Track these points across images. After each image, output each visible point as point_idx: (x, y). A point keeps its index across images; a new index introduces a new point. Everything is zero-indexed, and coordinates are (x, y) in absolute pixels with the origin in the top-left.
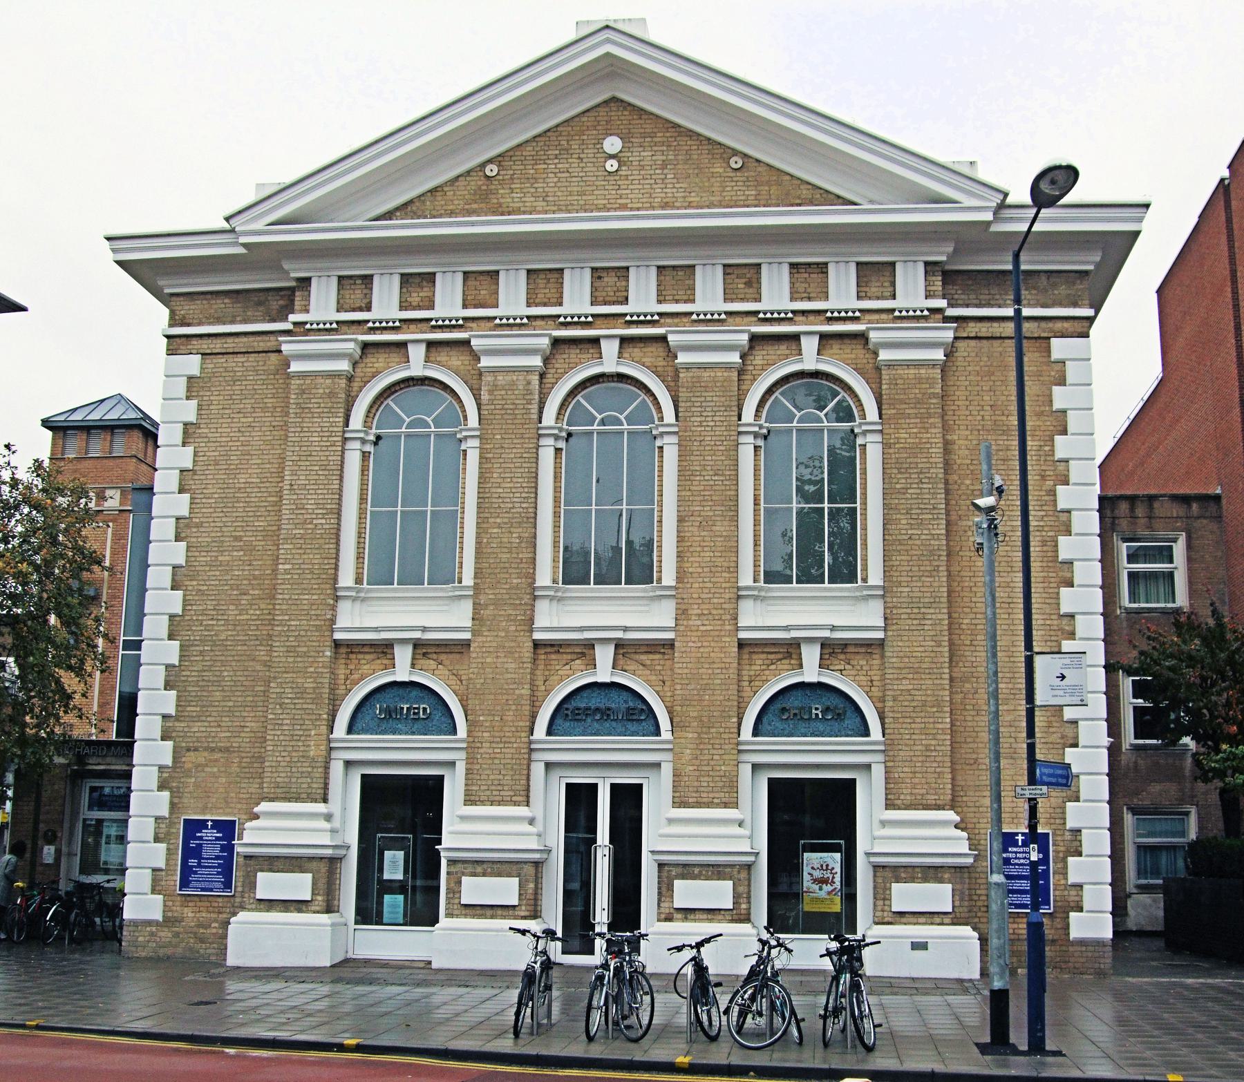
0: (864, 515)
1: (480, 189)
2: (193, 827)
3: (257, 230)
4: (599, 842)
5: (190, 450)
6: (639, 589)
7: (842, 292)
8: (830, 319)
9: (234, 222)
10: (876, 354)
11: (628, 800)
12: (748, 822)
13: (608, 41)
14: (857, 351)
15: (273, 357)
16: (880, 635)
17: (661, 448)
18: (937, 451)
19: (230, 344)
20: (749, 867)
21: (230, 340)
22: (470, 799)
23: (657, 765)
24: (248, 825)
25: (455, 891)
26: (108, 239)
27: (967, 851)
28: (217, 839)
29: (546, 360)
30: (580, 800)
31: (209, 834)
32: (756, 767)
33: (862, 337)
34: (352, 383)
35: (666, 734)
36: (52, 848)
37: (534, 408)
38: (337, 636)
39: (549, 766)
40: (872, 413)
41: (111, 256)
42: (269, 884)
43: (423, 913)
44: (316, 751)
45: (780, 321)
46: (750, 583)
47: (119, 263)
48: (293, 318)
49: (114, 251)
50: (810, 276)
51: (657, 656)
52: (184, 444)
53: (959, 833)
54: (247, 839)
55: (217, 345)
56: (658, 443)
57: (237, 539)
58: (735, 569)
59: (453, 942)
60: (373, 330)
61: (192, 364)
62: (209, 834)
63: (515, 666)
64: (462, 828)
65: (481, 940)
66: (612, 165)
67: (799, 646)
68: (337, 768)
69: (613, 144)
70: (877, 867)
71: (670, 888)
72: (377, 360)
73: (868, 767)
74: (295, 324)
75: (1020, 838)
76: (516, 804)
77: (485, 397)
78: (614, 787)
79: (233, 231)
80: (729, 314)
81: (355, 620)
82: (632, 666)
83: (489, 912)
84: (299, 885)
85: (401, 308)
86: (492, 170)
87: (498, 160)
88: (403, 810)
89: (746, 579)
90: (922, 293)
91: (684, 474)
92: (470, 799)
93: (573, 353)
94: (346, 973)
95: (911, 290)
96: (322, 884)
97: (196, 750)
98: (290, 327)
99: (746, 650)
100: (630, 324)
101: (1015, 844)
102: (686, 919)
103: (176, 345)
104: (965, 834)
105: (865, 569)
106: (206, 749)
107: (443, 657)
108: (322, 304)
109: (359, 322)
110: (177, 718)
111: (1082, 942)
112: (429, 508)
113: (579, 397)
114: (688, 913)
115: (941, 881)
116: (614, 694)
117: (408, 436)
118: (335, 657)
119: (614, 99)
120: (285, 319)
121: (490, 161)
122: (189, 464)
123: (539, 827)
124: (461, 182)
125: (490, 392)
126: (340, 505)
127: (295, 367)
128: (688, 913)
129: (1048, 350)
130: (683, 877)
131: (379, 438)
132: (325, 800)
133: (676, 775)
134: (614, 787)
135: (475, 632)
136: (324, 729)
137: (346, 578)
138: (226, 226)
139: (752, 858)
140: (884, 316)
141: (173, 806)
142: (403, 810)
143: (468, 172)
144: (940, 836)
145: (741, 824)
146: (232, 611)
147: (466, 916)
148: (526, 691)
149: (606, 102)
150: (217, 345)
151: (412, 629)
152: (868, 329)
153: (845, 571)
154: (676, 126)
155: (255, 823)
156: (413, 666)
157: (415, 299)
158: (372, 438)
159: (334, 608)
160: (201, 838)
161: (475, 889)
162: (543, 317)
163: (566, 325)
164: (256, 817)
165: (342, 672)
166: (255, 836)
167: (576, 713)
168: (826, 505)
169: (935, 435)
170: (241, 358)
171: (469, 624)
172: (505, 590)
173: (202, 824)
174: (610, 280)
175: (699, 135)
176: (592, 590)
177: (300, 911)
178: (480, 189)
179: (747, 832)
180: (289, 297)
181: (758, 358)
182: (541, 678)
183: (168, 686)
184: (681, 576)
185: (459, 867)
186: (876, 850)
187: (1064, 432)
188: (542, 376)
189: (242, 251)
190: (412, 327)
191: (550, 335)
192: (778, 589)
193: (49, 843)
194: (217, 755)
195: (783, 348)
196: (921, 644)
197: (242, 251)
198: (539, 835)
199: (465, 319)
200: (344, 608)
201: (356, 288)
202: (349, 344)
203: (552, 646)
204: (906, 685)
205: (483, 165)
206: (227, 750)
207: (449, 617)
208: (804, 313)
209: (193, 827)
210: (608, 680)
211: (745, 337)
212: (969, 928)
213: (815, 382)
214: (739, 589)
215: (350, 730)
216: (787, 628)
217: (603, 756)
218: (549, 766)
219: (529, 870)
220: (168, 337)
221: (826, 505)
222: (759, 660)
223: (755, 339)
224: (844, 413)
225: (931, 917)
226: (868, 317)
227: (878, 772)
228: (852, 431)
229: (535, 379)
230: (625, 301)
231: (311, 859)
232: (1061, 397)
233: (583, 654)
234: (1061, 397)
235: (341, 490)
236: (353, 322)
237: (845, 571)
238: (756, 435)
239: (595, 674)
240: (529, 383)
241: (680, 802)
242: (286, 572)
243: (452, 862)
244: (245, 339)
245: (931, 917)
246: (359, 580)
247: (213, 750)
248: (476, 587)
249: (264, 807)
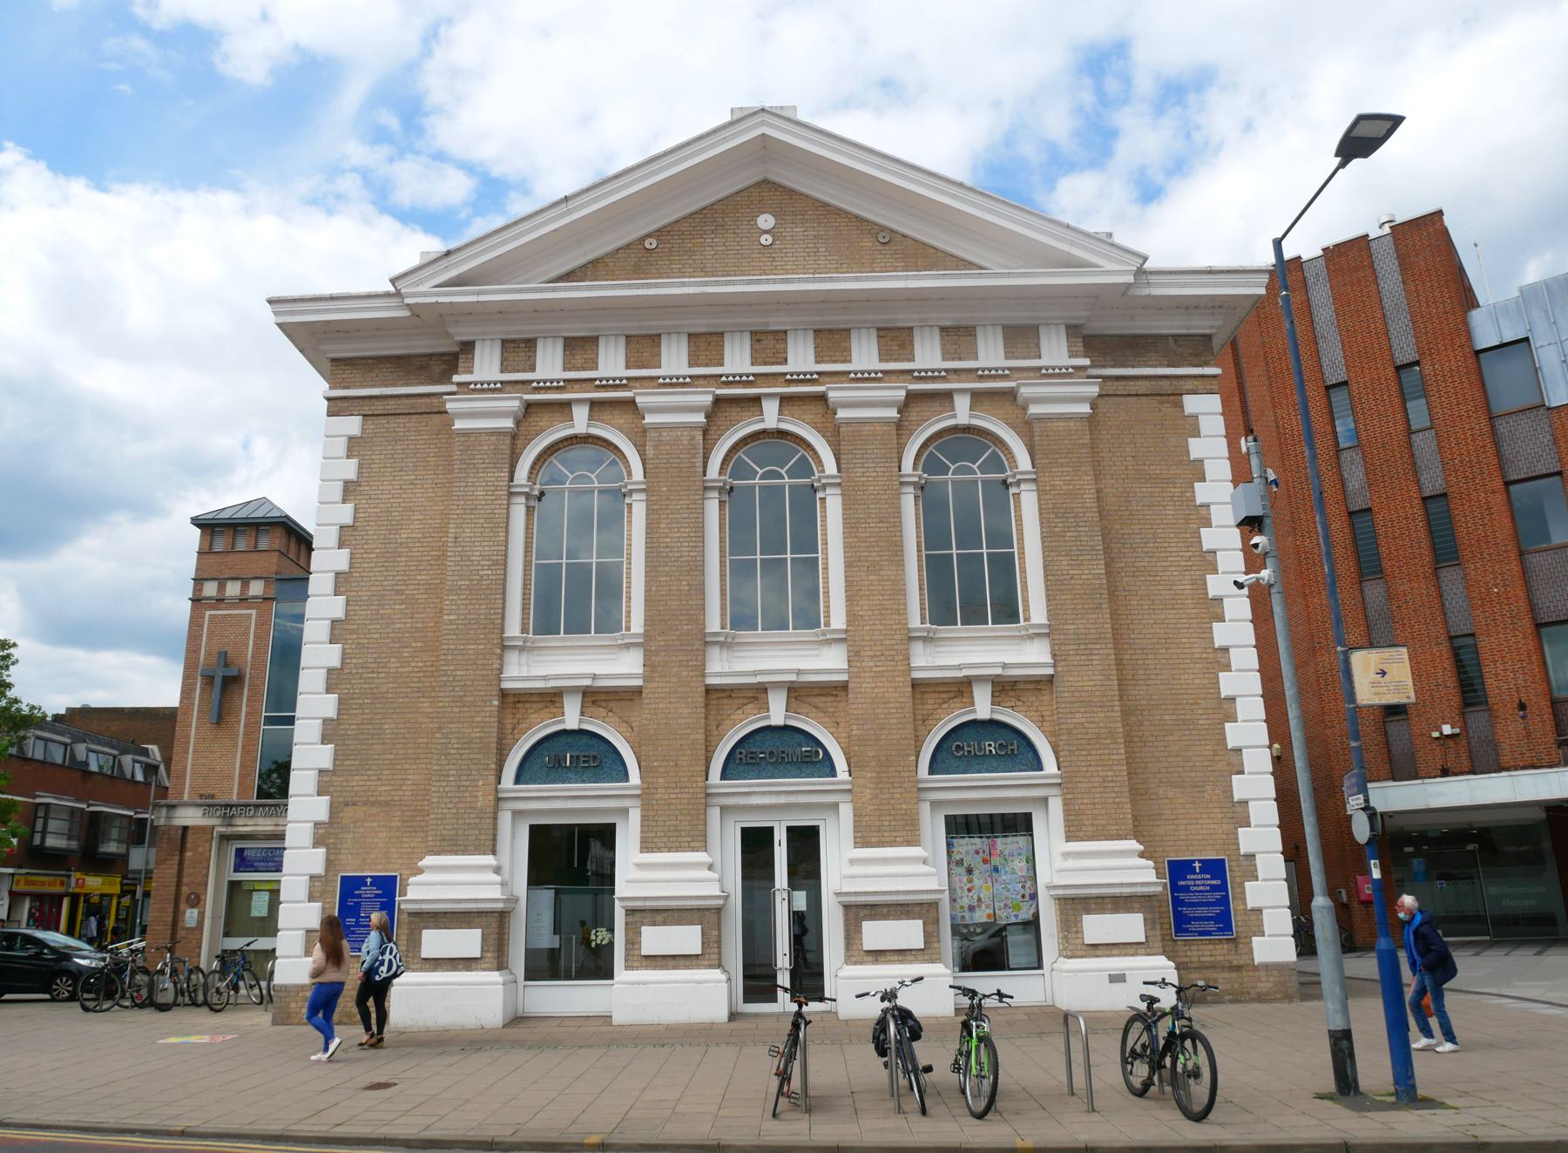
0: (1022, 558)
1: (635, 258)
2: (350, 886)
3: (424, 292)
4: (777, 886)
5: (349, 507)
6: (605, 639)
7: (801, 357)
8: (981, 377)
9: (399, 284)
10: (1025, 408)
11: (805, 842)
12: (718, 864)
13: (763, 123)
14: (814, 410)
15: (436, 418)
16: (1050, 671)
17: (630, 505)
18: (1089, 498)
19: (392, 406)
20: (718, 911)
21: (392, 402)
22: (647, 846)
23: (835, 806)
24: (412, 880)
25: (633, 942)
26: (270, 302)
27: (1153, 879)
28: (377, 896)
29: (518, 423)
30: (756, 843)
31: (368, 891)
32: (517, 814)
33: (822, 398)
34: (515, 441)
35: (635, 777)
36: (195, 911)
37: (699, 461)
38: (505, 685)
39: (724, 809)
40: (1024, 462)
41: (273, 319)
42: (434, 942)
43: (598, 966)
44: (484, 801)
45: (933, 379)
46: (718, 629)
47: (280, 325)
48: (456, 378)
49: (276, 313)
50: (769, 343)
51: (830, 699)
52: (344, 501)
53: (1143, 862)
54: (412, 894)
55: (379, 407)
56: (627, 500)
57: (398, 592)
58: (902, 611)
59: (630, 995)
60: (538, 390)
61: (352, 425)
62: (368, 891)
63: (687, 712)
64: (637, 873)
65: (669, 989)
66: (766, 240)
67: (765, 690)
68: (505, 819)
69: (766, 221)
70: (847, 907)
71: (859, 930)
72: (542, 419)
73: (1045, 800)
74: (459, 384)
75: (1197, 865)
76: (694, 849)
77: (650, 452)
78: (790, 830)
79: (398, 294)
80: (885, 372)
81: (521, 672)
82: (612, 717)
83: (671, 963)
84: (468, 941)
85: (565, 369)
86: (651, 243)
87: (658, 233)
88: (571, 862)
89: (915, 621)
90: (812, 358)
91: (850, 524)
92: (647, 846)
93: (734, 411)
94: (518, 1032)
95: (1055, 351)
96: (492, 940)
97: (355, 804)
98: (454, 388)
99: (918, 690)
100: (790, 382)
101: (1193, 871)
102: (876, 962)
103: (336, 407)
104: (1151, 863)
105: (1026, 609)
106: (365, 804)
107: (612, 705)
108: (486, 365)
109: (523, 382)
110: (333, 772)
111: (1267, 967)
112: (954, 551)
113: (740, 453)
114: (878, 955)
115: (1130, 910)
116: (787, 736)
117: (571, 491)
118: (502, 708)
119: (766, 181)
120: (449, 381)
121: (649, 235)
122: (348, 520)
123: (708, 873)
124: (621, 254)
125: (656, 447)
126: (506, 556)
127: (459, 425)
128: (878, 955)
129: (1180, 405)
130: (872, 918)
131: (542, 494)
132: (494, 853)
133: (858, 816)
134: (790, 830)
135: (646, 679)
136: (492, 779)
137: (513, 629)
138: (391, 289)
139: (721, 902)
140: (1031, 374)
141: (329, 863)
142: (571, 862)
143: (628, 246)
144: (1127, 866)
145: (710, 867)
146: (394, 664)
147: (646, 968)
148: (701, 736)
149: (758, 184)
150: (379, 407)
151: (993, 665)
152: (1019, 386)
153: (1008, 611)
154: (827, 205)
155: (419, 878)
156: (582, 714)
157: (578, 360)
158: (536, 493)
159: (501, 658)
160: (359, 896)
161: (656, 939)
162: (705, 377)
163: (728, 384)
164: (421, 871)
165: (509, 721)
166: (419, 891)
167: (750, 757)
168: (789, 556)
169: (1087, 482)
170: (402, 420)
171: (1049, 660)
172: (874, 635)
173: (360, 881)
174: (769, 342)
175: (847, 213)
176: (564, 640)
177: (468, 969)
178: (635, 258)
179: (716, 876)
180: (452, 360)
181: (913, 415)
182: (714, 723)
183: (325, 740)
184: (851, 617)
185: (637, 917)
186: (845, 890)
187: (1203, 479)
188: (705, 432)
189: (406, 313)
190: (576, 387)
191: (521, 399)
192: (744, 635)
193: (193, 906)
194: (375, 810)
195: (936, 405)
196: (1092, 679)
197: (406, 313)
198: (502, 884)
199: (628, 379)
200: (512, 658)
201: (519, 350)
202: (513, 403)
203: (724, 690)
204: (1078, 718)
205: (642, 239)
206: (388, 804)
207: (622, 666)
208: (955, 371)
209: (350, 886)
210: (575, 727)
211: (710, 398)
212: (718, 971)
213: (967, 440)
214: (910, 630)
215: (518, 781)
216: (755, 673)
217: (775, 800)
218: (724, 809)
219: (706, 915)
220: (328, 399)
221: (954, 551)
222: (931, 700)
223: (529, 406)
224: (803, 469)
225: (902, 954)
226: (1016, 375)
227: (1056, 805)
228: (1004, 482)
229: (699, 438)
230: (785, 361)
231: (481, 913)
232: (350, 469)
233: (756, 698)
234: (350, 469)
235: (506, 541)
236: (517, 382)
237: (1008, 611)
238: (721, 490)
239: (768, 717)
240: (693, 438)
241: (862, 841)
242: (451, 622)
243: (630, 912)
244: (406, 401)
245: (902, 954)
246: (524, 630)
247: (373, 804)
248: (646, 634)
249: (429, 860)
